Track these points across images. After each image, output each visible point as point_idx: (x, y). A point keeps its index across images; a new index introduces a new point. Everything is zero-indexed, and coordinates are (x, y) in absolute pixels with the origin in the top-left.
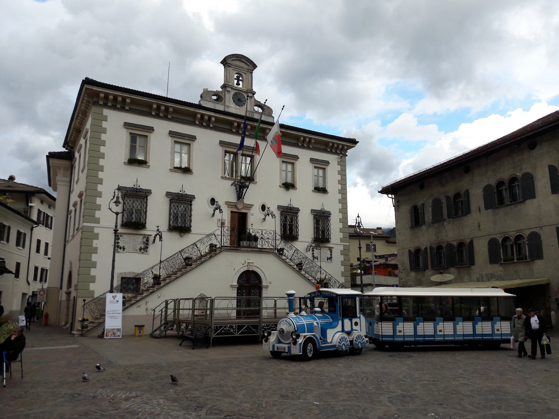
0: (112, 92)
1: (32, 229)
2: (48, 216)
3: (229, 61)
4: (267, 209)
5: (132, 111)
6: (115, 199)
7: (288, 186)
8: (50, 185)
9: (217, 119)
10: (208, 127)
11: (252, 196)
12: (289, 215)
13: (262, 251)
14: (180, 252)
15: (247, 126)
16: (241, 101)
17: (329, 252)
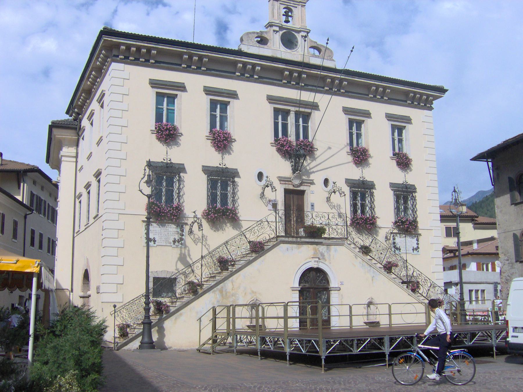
1: (25, 217)
2: (41, 200)
4: (264, 178)
6: (146, 178)
8: (48, 162)
9: (263, 67)
10: (251, 79)
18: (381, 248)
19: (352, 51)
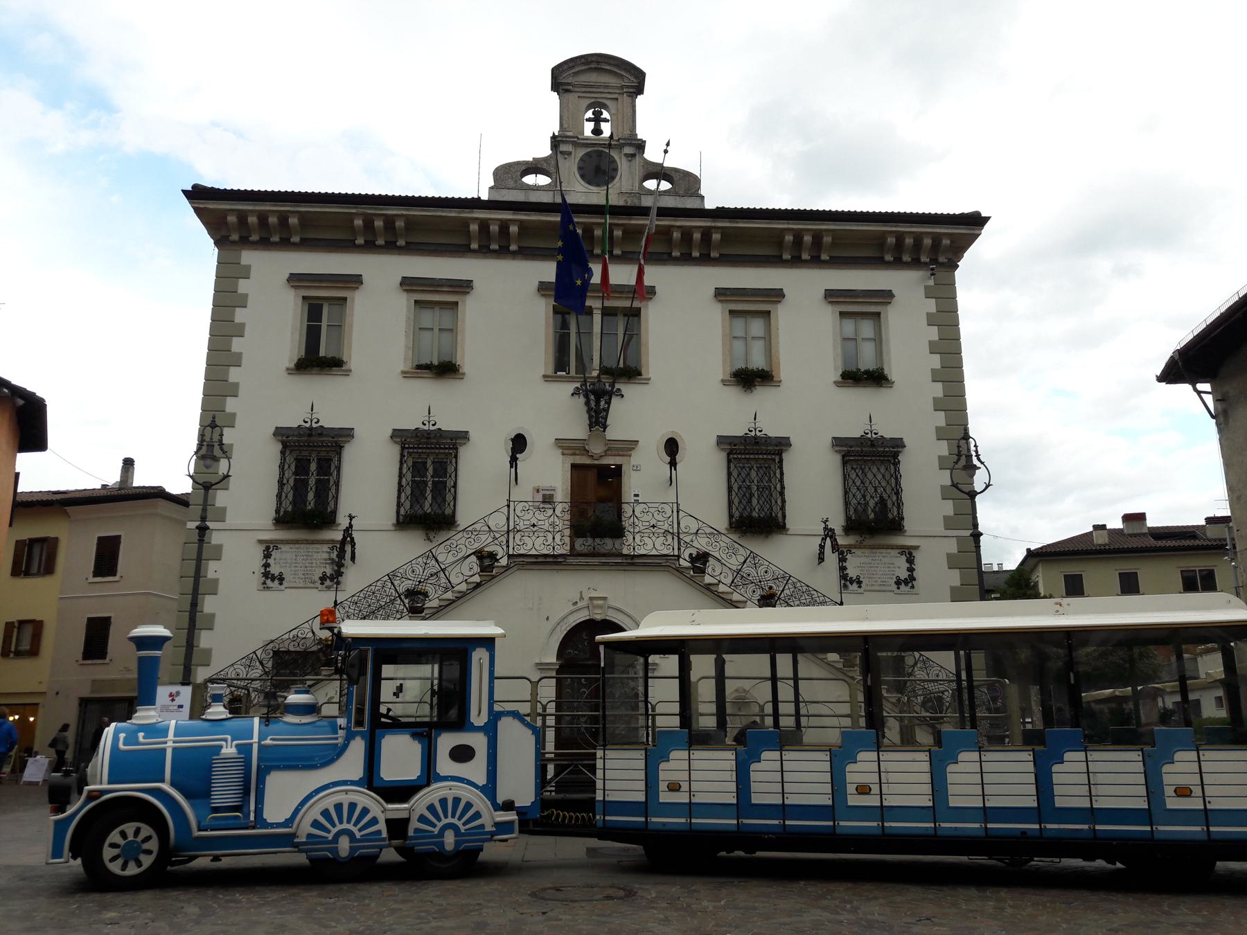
0: (251, 208)
3: (566, 78)
5: (309, 244)
7: (749, 379)
9: (410, 222)
10: (503, 252)
11: (636, 416)
12: (755, 463)
13: (636, 563)
14: (391, 577)
15: (802, 238)
16: (604, 173)
17: (902, 562)
18: (769, 576)
19: (666, 152)
